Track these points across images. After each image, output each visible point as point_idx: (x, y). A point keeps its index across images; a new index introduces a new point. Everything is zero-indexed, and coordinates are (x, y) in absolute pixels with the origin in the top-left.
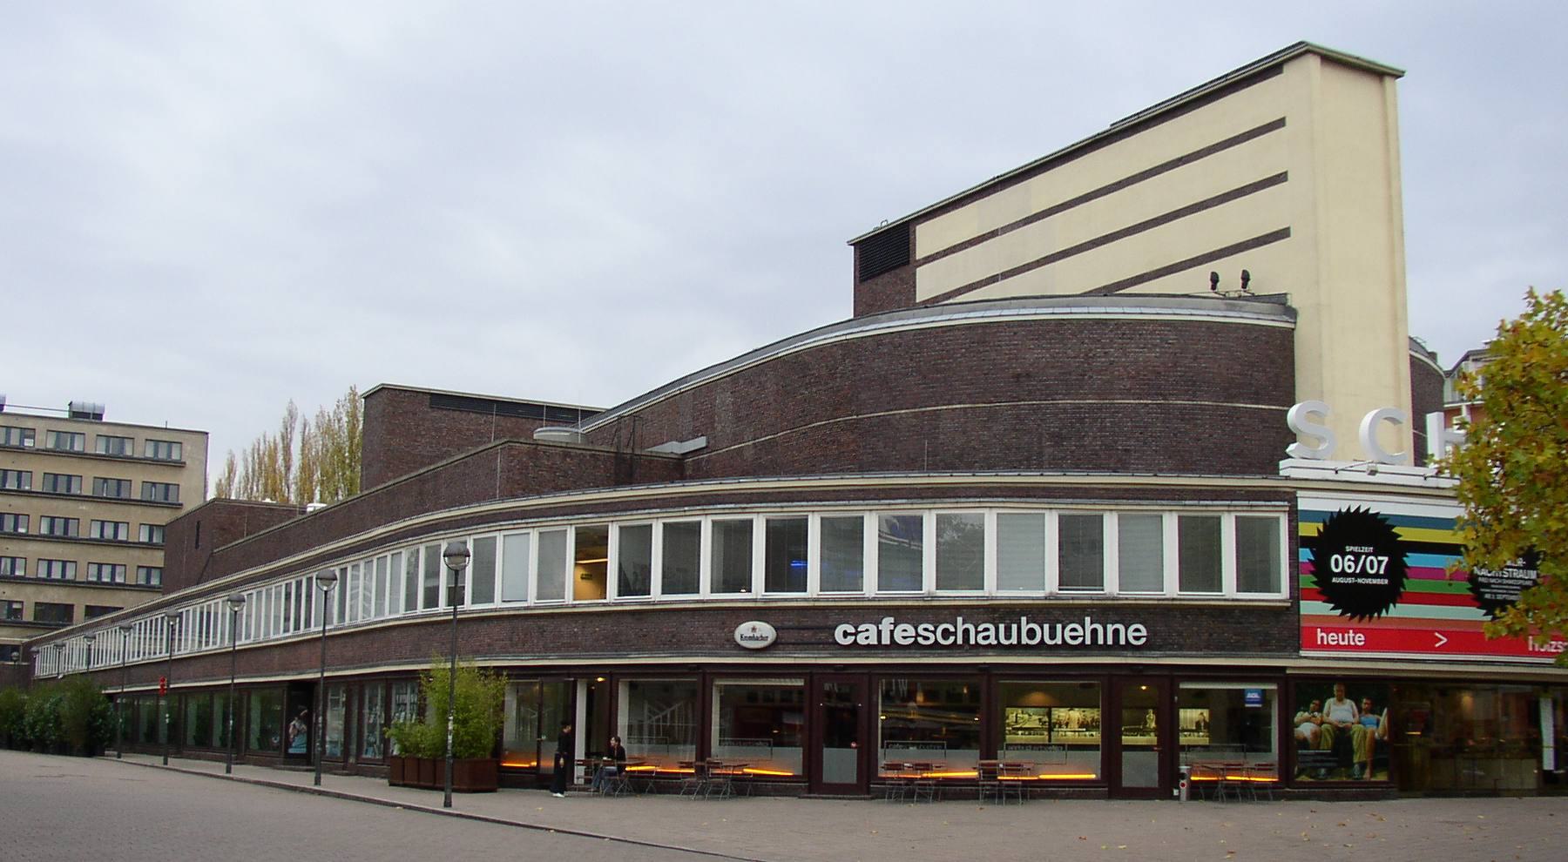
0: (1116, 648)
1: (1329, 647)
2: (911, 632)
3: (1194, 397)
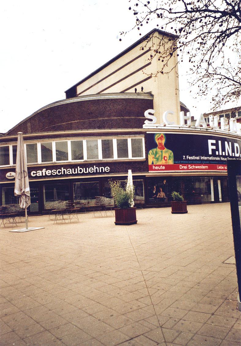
3: (130, 116)
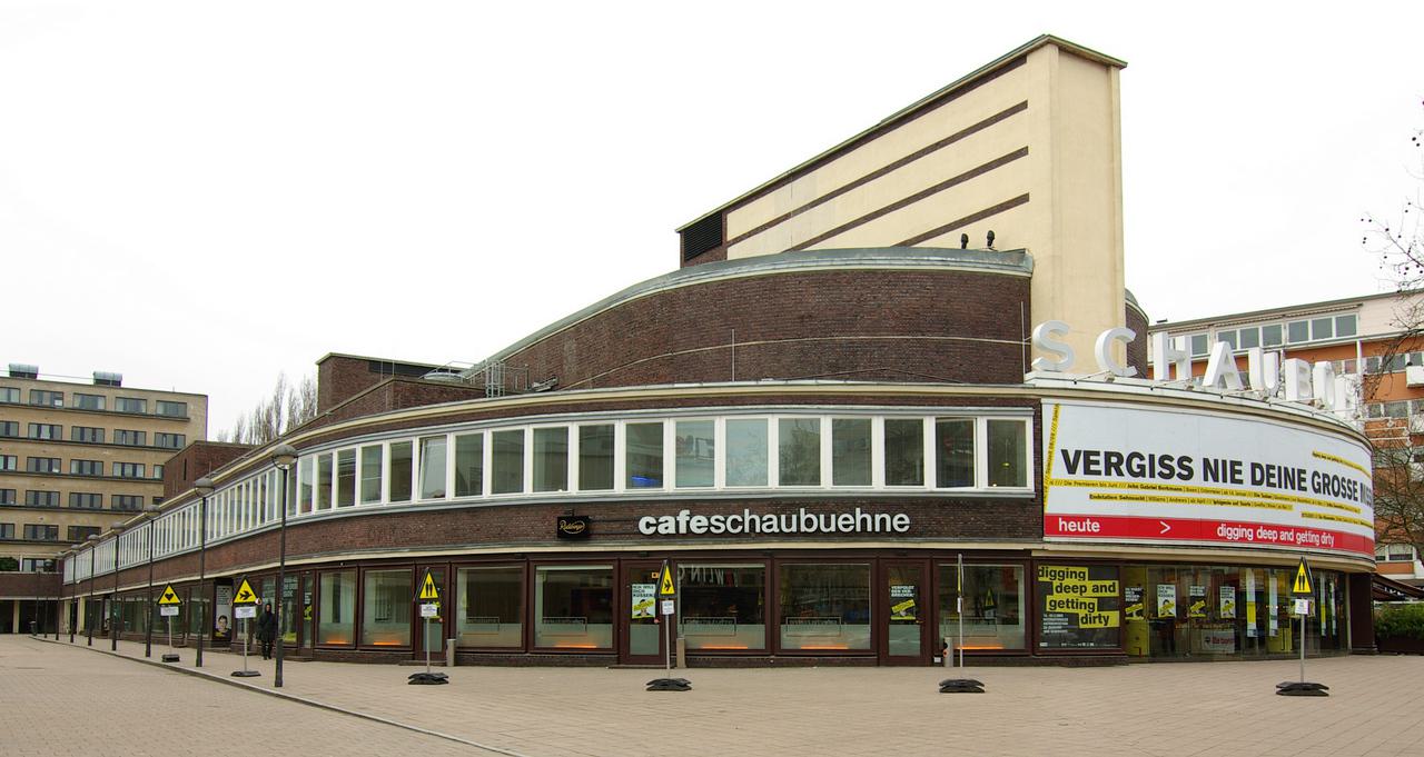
0: (883, 534)
1: (1069, 533)
2: (705, 522)
3: (947, 333)
